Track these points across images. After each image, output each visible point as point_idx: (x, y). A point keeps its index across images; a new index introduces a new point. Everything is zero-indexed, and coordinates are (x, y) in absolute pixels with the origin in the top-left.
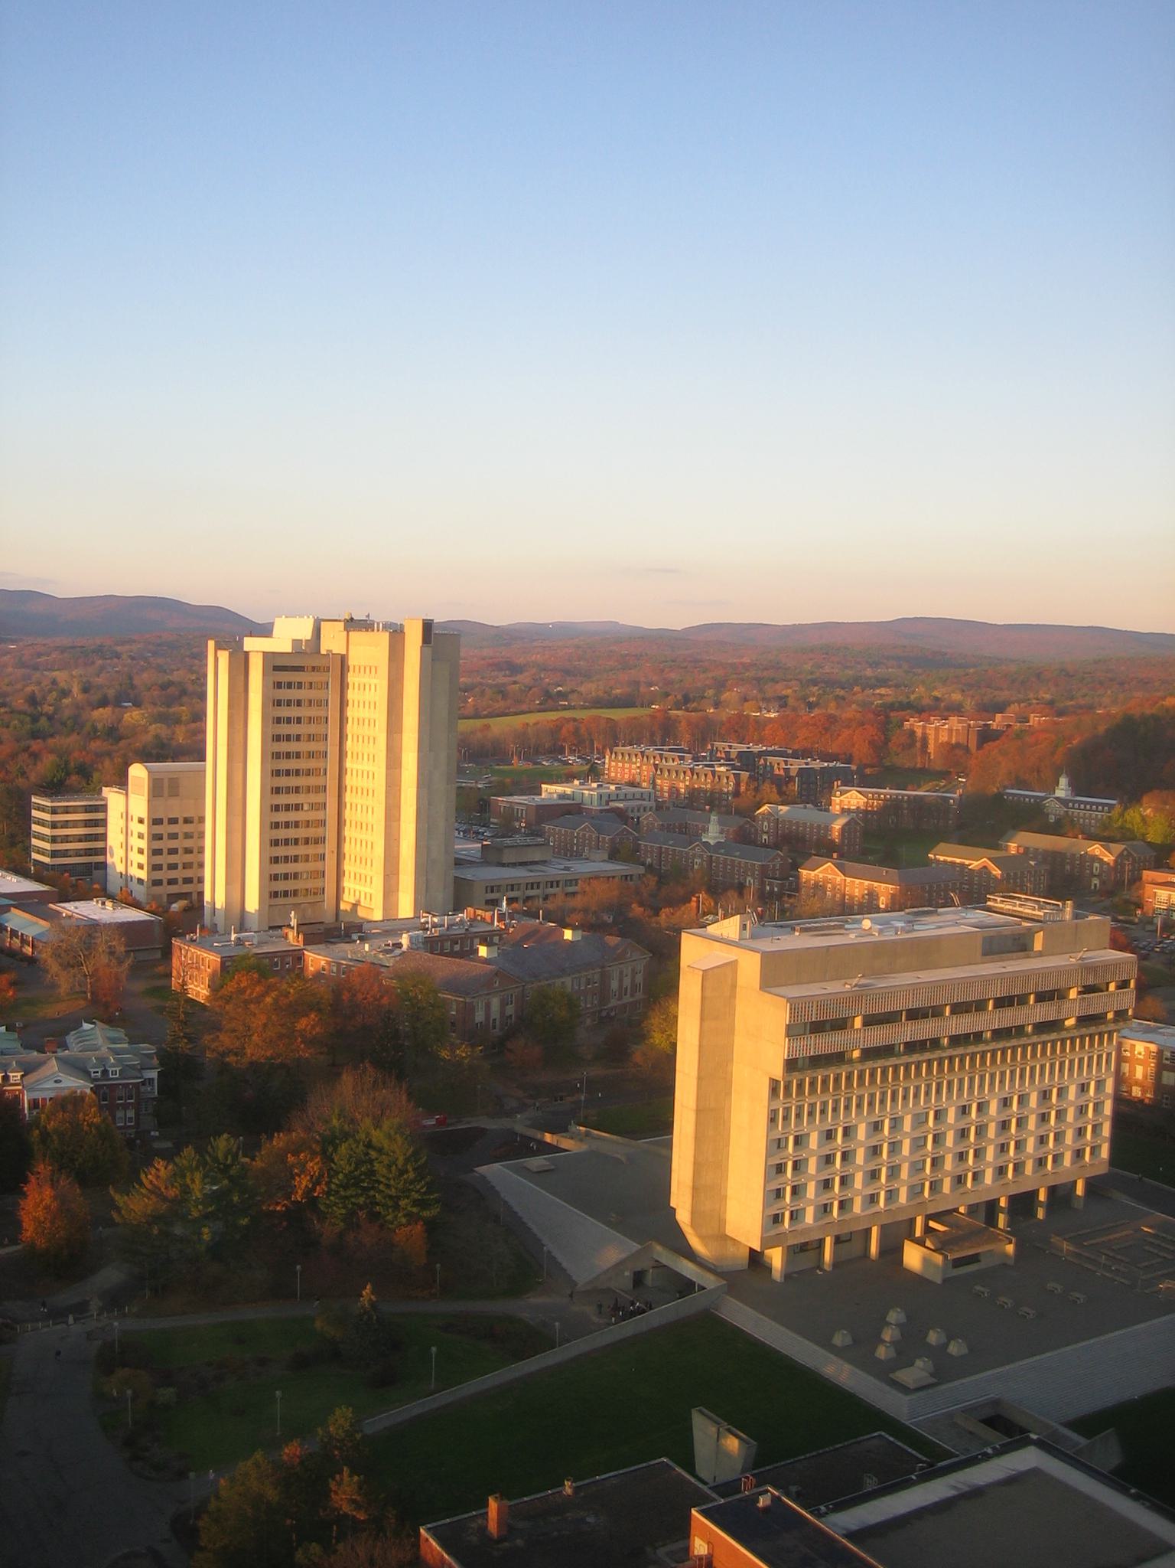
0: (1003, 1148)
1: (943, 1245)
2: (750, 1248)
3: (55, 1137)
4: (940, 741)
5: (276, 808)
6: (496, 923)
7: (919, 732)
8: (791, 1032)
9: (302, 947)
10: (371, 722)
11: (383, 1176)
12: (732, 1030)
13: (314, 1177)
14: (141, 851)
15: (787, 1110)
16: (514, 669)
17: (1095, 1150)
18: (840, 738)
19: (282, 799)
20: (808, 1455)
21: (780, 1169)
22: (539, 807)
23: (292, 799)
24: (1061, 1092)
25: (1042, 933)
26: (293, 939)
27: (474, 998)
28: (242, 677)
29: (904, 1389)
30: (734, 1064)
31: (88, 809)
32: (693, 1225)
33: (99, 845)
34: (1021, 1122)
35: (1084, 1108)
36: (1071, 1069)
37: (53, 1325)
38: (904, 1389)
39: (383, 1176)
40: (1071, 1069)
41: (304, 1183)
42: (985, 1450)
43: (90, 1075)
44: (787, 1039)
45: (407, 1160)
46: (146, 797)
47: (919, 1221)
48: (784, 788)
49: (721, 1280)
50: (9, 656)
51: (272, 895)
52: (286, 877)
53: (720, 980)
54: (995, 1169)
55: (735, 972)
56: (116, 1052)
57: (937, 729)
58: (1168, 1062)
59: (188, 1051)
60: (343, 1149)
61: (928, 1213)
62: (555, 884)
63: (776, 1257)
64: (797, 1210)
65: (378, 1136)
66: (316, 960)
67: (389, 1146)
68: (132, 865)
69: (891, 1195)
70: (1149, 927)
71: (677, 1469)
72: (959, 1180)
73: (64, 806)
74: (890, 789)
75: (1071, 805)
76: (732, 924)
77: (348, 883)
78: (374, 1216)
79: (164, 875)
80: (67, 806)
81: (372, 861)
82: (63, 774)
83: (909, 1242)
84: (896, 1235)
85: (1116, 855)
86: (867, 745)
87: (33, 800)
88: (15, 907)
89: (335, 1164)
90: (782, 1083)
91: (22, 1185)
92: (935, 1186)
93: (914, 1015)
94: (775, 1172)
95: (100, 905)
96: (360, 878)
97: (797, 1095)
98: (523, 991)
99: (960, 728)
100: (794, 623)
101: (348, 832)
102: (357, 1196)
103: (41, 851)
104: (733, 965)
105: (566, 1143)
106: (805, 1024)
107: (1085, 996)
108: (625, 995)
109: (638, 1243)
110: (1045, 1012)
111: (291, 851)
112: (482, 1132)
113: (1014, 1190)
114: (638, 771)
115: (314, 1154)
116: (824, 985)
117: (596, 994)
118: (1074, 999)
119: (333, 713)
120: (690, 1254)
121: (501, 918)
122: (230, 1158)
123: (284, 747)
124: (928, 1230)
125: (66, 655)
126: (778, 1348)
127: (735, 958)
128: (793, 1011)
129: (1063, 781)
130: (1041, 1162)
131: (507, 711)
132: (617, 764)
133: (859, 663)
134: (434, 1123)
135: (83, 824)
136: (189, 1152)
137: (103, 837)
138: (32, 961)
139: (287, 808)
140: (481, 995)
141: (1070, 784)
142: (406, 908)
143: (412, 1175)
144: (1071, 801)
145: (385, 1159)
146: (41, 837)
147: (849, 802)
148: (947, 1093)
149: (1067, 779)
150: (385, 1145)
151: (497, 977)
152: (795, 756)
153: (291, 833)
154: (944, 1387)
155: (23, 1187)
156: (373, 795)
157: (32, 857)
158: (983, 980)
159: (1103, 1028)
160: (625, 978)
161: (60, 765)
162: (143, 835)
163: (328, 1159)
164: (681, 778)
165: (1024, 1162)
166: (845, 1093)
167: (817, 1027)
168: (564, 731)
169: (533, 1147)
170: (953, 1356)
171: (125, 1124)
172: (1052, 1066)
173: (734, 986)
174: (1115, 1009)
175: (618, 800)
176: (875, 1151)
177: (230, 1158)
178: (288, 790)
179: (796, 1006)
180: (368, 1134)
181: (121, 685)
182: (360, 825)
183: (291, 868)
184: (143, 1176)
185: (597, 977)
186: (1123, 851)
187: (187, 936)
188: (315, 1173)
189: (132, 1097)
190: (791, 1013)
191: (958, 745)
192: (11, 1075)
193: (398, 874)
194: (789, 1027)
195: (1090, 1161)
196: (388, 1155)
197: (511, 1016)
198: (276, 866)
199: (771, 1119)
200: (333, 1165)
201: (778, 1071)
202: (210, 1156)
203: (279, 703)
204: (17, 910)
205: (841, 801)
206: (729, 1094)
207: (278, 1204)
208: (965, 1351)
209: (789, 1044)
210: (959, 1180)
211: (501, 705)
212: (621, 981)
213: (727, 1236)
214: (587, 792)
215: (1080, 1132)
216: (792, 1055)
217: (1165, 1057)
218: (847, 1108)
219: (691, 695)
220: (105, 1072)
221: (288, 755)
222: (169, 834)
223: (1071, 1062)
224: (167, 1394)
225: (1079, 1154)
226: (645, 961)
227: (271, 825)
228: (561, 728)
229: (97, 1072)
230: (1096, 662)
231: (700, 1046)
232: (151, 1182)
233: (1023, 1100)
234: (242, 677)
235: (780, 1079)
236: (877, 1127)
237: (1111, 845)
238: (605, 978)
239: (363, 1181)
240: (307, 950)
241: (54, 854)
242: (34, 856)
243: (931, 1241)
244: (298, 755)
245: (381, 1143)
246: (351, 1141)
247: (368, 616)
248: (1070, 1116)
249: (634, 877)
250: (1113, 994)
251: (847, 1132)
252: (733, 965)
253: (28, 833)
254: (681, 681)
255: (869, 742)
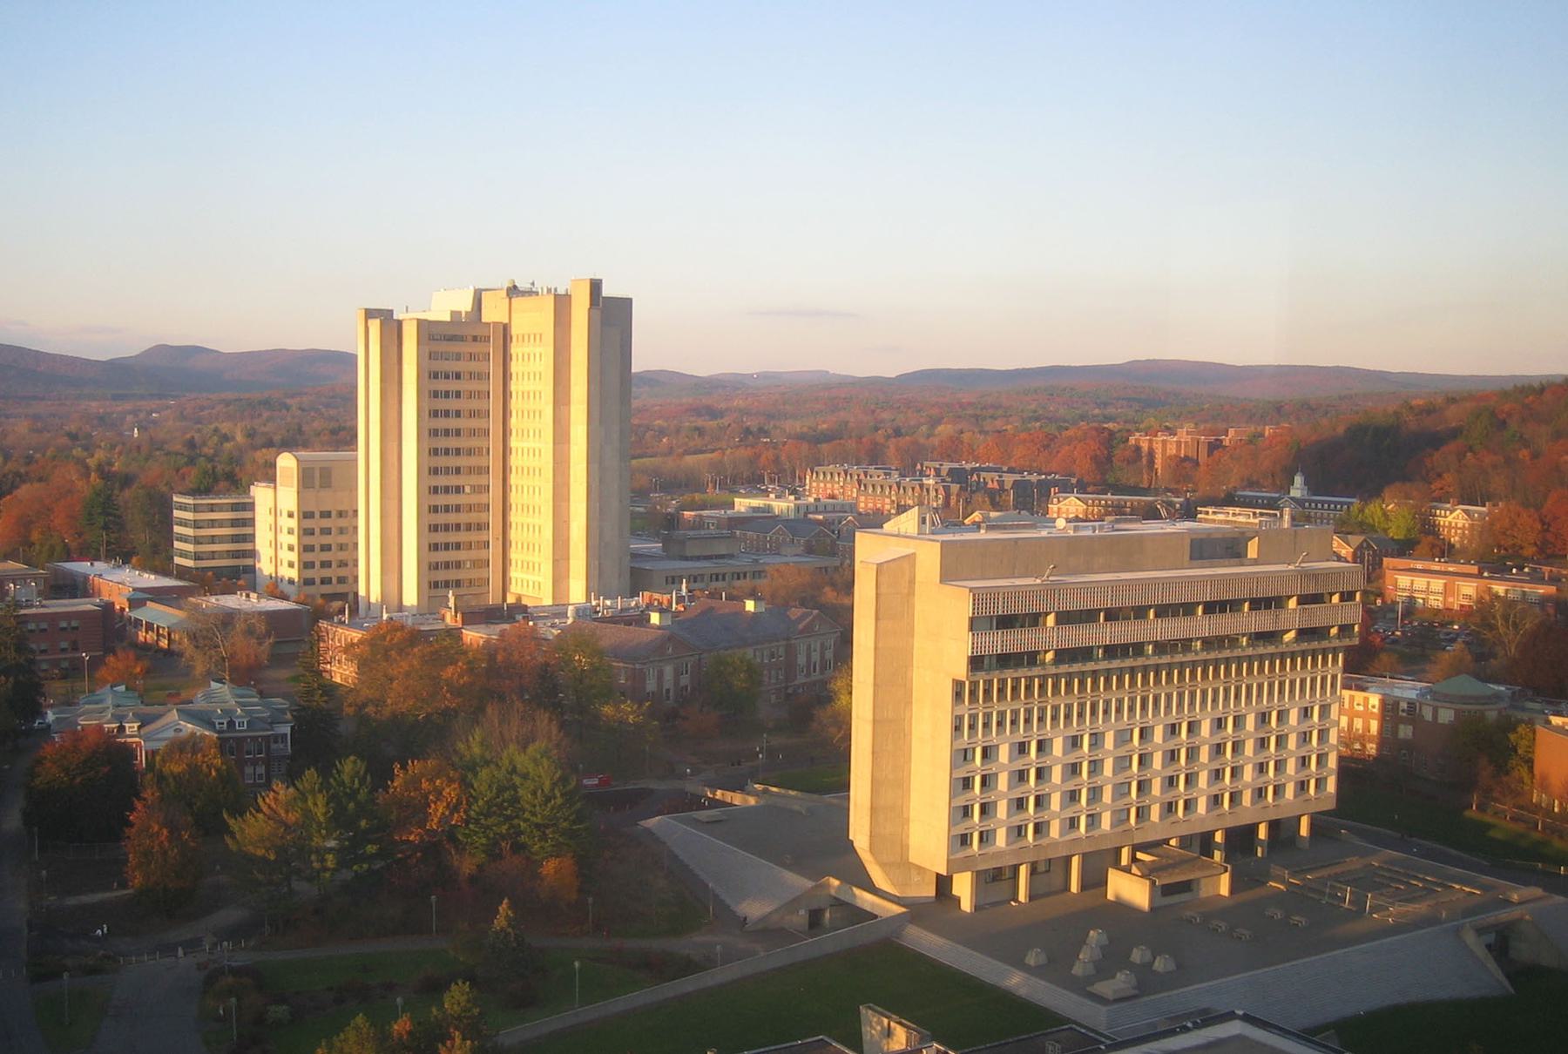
0: (1217, 775)
1: (1148, 873)
2: (937, 874)
3: (171, 780)
4: (1168, 454)
5: (435, 490)
6: (674, 606)
7: (1145, 446)
8: (973, 624)
9: (460, 626)
10: (537, 395)
11: (528, 803)
12: (911, 633)
13: (451, 805)
14: (291, 548)
15: (973, 718)
16: (713, 413)
17: (1320, 783)
18: (1059, 455)
19: (442, 481)
20: (988, 1045)
21: (967, 783)
22: (730, 519)
23: (453, 481)
24: (1282, 716)
25: (1257, 538)
26: (450, 619)
27: (645, 664)
28: (395, 348)
29: (1100, 999)
30: (915, 669)
31: (235, 507)
32: (872, 850)
33: (247, 546)
34: (1237, 747)
35: (1308, 735)
36: (1292, 691)
37: (160, 958)
38: (1100, 999)
39: (528, 803)
40: (1292, 691)
41: (441, 811)
42: (1184, 1023)
43: (215, 727)
44: (970, 633)
45: (554, 785)
46: (295, 489)
47: (1125, 853)
48: (997, 499)
50: (169, 411)
51: (433, 586)
52: (447, 565)
53: (896, 574)
54: (1208, 798)
55: (913, 566)
56: (242, 705)
57: (1164, 443)
58: (1404, 714)
59: (323, 705)
60: (484, 773)
61: (1135, 842)
62: (742, 575)
63: (963, 887)
64: (988, 831)
65: (522, 761)
66: (473, 636)
67: (534, 770)
68: (281, 564)
69: (1093, 820)
70: (1390, 615)
71: (834, 1044)
72: (1170, 808)
73: (208, 504)
74: (1112, 494)
75: (1307, 504)
76: (909, 517)
77: (514, 573)
78: (518, 848)
79: (317, 573)
80: (212, 504)
81: (540, 547)
82: (211, 480)
83: (1114, 871)
84: (1099, 864)
85: (1354, 547)
86: (1089, 461)
87: (175, 499)
88: (152, 600)
89: (475, 790)
90: (967, 683)
91: (128, 813)
92: (1142, 813)
93: (1112, 615)
94: (961, 787)
95: (244, 598)
96: (528, 566)
97: (984, 702)
98: (700, 660)
99: (1189, 440)
100: (1017, 367)
101: (514, 517)
102: (499, 824)
103: (184, 553)
104: (911, 558)
105: (737, 799)
106: (991, 617)
107: (1306, 606)
108: (815, 672)
109: (810, 879)
110: (1263, 621)
111: (453, 537)
112: (652, 791)
113: (1231, 823)
114: (841, 491)
115: (451, 781)
116: (1013, 580)
117: (781, 669)
118: (1293, 610)
119: (494, 368)
120: (871, 887)
121: (680, 599)
122: (356, 782)
123: (442, 423)
124: (1134, 860)
125: (231, 407)
126: (965, 971)
127: (912, 551)
128: (976, 601)
129: (1298, 480)
130: (1260, 793)
131: (704, 448)
132: (818, 485)
133: (1086, 404)
134: (597, 782)
135: (229, 523)
136: (311, 775)
137: (251, 538)
138: (169, 653)
139: (447, 490)
140: (651, 662)
141: (1306, 483)
142: (577, 592)
143: (559, 801)
144: (1306, 501)
145: (530, 785)
146: (184, 523)
147: (1068, 510)
148: (1153, 709)
149: (1303, 478)
150: (530, 770)
151: (670, 640)
152: (1011, 471)
153: (452, 518)
154: (1146, 999)
155: (129, 816)
156: (540, 475)
157: (175, 562)
158: (1191, 581)
159: (1325, 644)
160: (813, 654)
161: (207, 472)
162: (293, 529)
163: (465, 784)
164: (887, 493)
165: (1241, 792)
166: (1039, 702)
167: (1006, 622)
168: (763, 459)
169: (704, 803)
170: (1159, 973)
171: (255, 780)
172: (1271, 686)
173: (912, 582)
174: (1339, 623)
175: (817, 512)
176: (1074, 769)
177: (356, 782)
178: (447, 471)
179: (978, 597)
180: (511, 761)
181: (288, 431)
182: (526, 508)
183: (452, 555)
184: (260, 800)
185: (781, 651)
186: (1362, 542)
187: (335, 618)
188: (452, 800)
189: (262, 750)
190: (974, 604)
191: (1187, 458)
192: (127, 725)
193: (568, 559)
194: (972, 620)
195: (1315, 794)
196: (533, 780)
197: (687, 686)
198: (436, 553)
199: (956, 727)
200: (472, 791)
201: (961, 670)
202: (335, 779)
203: (436, 376)
204: (157, 605)
205: (1059, 509)
206: (909, 703)
207: (411, 833)
208: (1171, 966)
209: (973, 639)
210: (1170, 808)
211: (698, 442)
212: (809, 657)
213: (911, 863)
214: (782, 505)
215: (1304, 762)
216: (977, 652)
217: (1401, 709)
218: (1041, 719)
219: (903, 431)
220: (231, 724)
221: (447, 432)
222: (321, 512)
223: (1292, 683)
224: (279, 1011)
225: (1302, 786)
226: (835, 635)
227: (429, 509)
228: (760, 456)
229: (223, 724)
230: (1341, 398)
231: (876, 648)
232: (269, 807)
233: (1239, 721)
234: (396, 349)
235: (964, 679)
236: (1075, 742)
237: (1349, 536)
238: (791, 651)
239: (506, 809)
240: (465, 629)
241: (197, 557)
242: (177, 560)
243: (1138, 868)
244: (458, 433)
245: (526, 768)
246: (492, 766)
247: (533, 284)
248: (1292, 742)
249: (829, 570)
250: (1335, 606)
251: (1041, 746)
252: (911, 558)
253: (169, 537)
254: (893, 420)
255: (1091, 459)
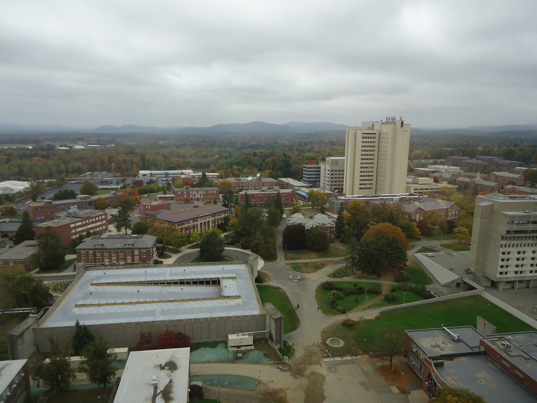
49: (471, 350)
198: (362, 169)
